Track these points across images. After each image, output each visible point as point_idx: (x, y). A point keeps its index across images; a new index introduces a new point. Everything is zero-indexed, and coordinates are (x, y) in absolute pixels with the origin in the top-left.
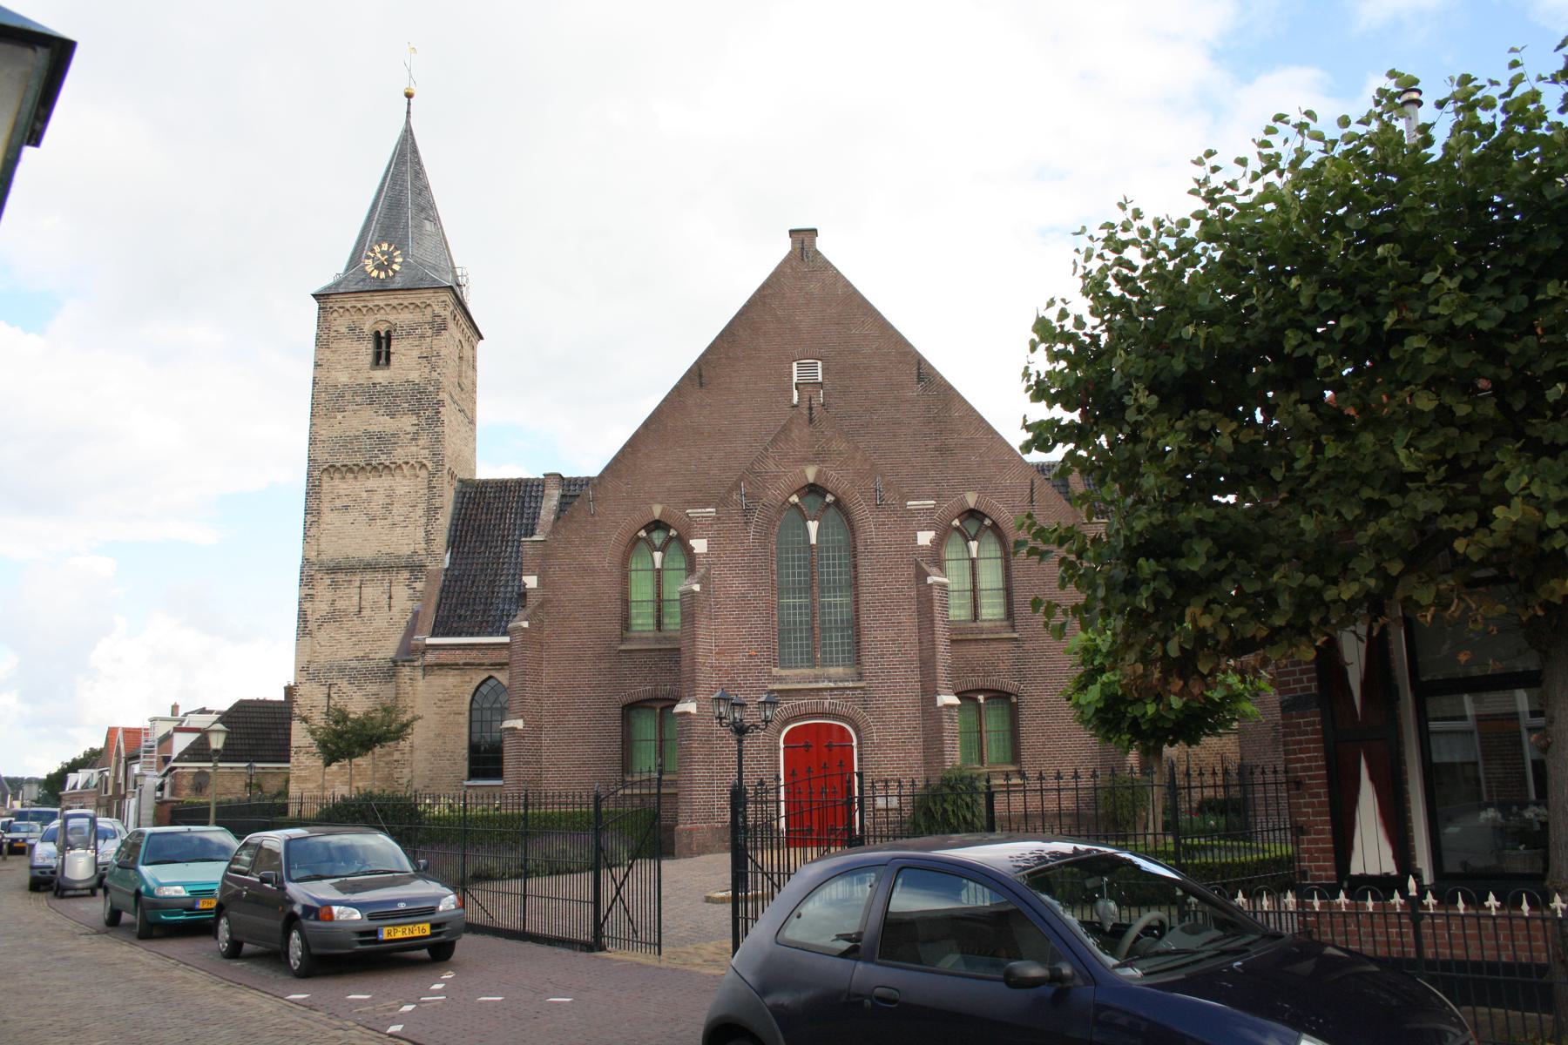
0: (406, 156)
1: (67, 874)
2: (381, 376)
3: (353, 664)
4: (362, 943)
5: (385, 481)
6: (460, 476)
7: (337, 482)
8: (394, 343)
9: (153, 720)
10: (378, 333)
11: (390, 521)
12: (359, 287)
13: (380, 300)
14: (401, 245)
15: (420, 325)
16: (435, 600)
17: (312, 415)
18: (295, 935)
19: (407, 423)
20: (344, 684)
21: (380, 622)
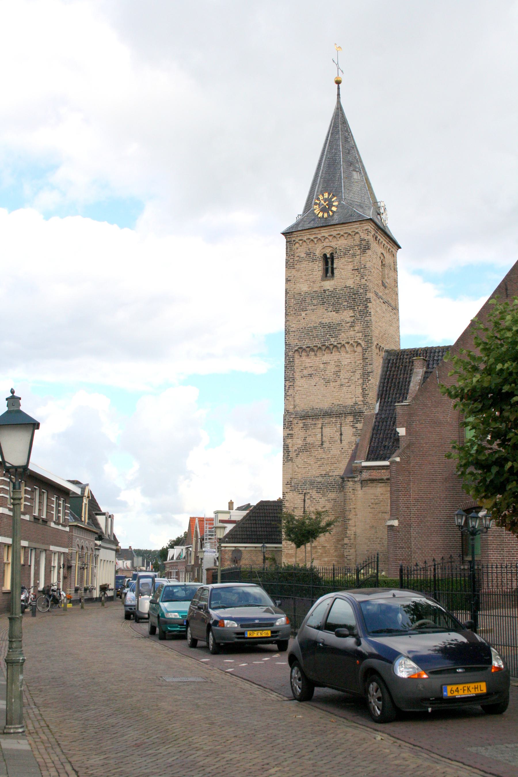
0: (339, 127)
1: (140, 610)
2: (328, 285)
3: (319, 479)
4: (239, 638)
5: (335, 356)
6: (387, 348)
7: (304, 358)
8: (335, 261)
9: (217, 513)
10: (325, 255)
11: (338, 383)
12: (311, 225)
13: (325, 233)
14: (336, 193)
15: (352, 247)
16: (368, 435)
17: (286, 315)
18: (211, 634)
19: (347, 315)
20: (314, 493)
21: (335, 451)
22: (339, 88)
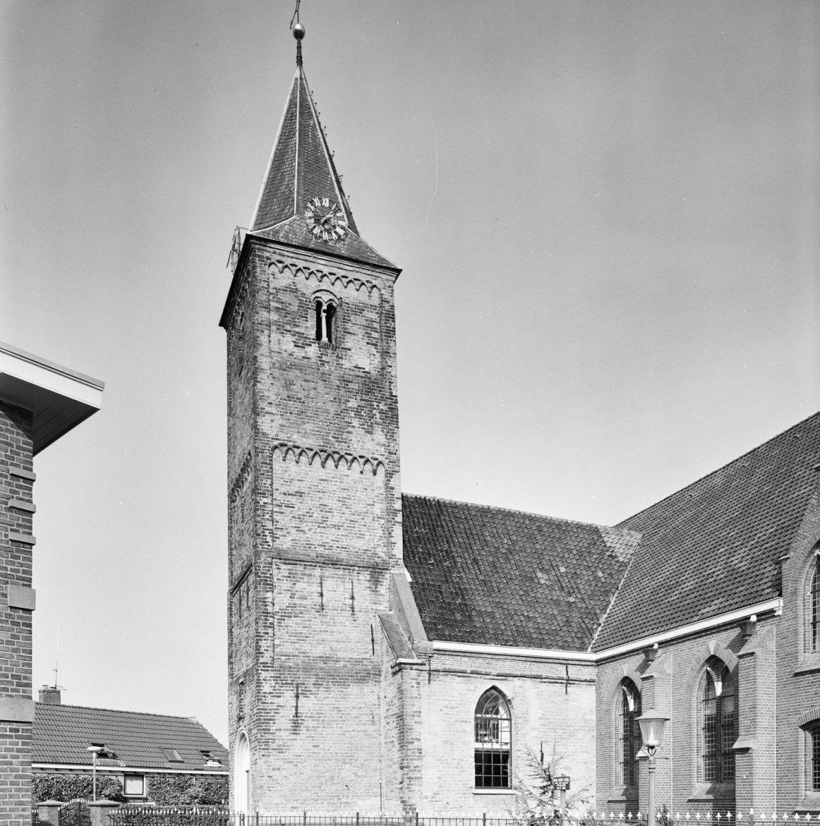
22: (299, 47)
